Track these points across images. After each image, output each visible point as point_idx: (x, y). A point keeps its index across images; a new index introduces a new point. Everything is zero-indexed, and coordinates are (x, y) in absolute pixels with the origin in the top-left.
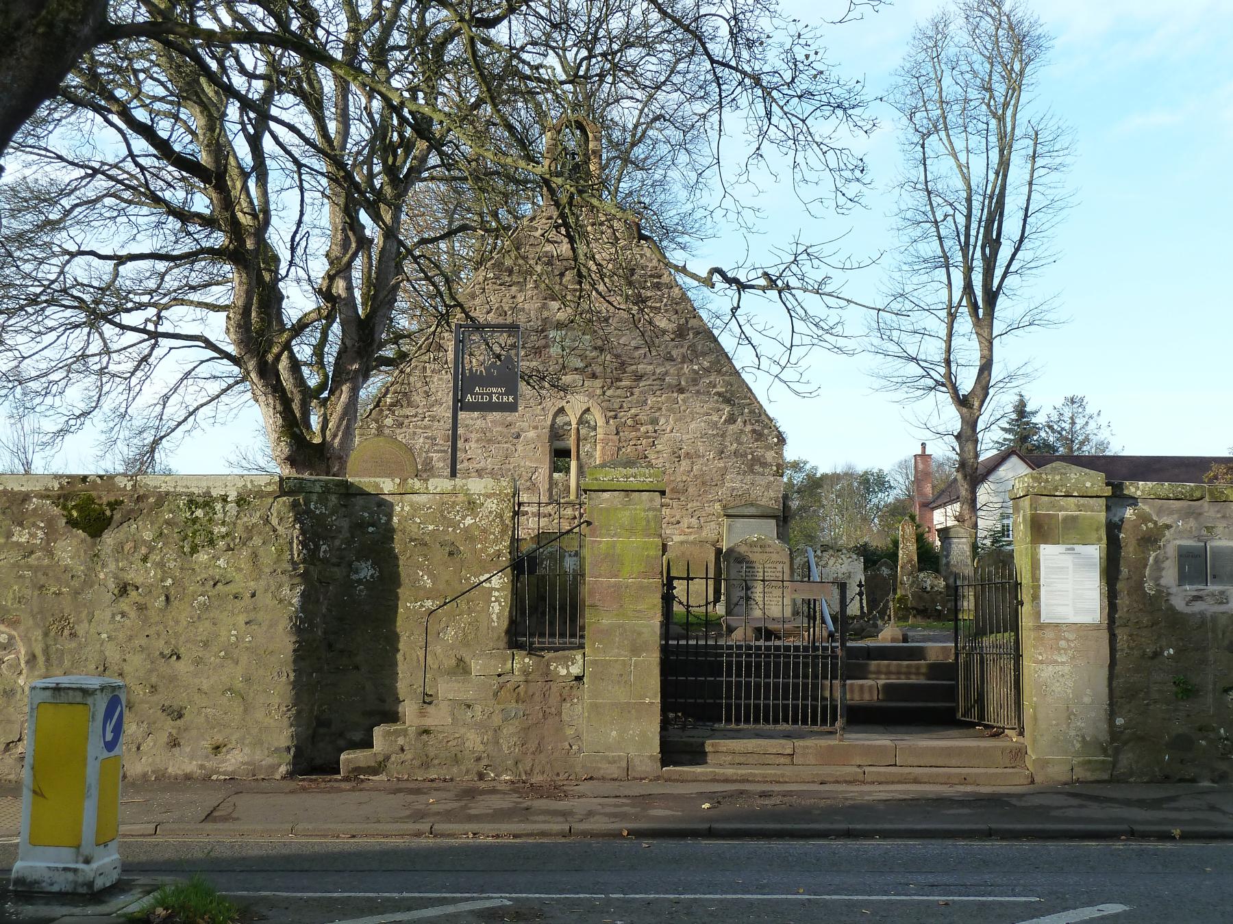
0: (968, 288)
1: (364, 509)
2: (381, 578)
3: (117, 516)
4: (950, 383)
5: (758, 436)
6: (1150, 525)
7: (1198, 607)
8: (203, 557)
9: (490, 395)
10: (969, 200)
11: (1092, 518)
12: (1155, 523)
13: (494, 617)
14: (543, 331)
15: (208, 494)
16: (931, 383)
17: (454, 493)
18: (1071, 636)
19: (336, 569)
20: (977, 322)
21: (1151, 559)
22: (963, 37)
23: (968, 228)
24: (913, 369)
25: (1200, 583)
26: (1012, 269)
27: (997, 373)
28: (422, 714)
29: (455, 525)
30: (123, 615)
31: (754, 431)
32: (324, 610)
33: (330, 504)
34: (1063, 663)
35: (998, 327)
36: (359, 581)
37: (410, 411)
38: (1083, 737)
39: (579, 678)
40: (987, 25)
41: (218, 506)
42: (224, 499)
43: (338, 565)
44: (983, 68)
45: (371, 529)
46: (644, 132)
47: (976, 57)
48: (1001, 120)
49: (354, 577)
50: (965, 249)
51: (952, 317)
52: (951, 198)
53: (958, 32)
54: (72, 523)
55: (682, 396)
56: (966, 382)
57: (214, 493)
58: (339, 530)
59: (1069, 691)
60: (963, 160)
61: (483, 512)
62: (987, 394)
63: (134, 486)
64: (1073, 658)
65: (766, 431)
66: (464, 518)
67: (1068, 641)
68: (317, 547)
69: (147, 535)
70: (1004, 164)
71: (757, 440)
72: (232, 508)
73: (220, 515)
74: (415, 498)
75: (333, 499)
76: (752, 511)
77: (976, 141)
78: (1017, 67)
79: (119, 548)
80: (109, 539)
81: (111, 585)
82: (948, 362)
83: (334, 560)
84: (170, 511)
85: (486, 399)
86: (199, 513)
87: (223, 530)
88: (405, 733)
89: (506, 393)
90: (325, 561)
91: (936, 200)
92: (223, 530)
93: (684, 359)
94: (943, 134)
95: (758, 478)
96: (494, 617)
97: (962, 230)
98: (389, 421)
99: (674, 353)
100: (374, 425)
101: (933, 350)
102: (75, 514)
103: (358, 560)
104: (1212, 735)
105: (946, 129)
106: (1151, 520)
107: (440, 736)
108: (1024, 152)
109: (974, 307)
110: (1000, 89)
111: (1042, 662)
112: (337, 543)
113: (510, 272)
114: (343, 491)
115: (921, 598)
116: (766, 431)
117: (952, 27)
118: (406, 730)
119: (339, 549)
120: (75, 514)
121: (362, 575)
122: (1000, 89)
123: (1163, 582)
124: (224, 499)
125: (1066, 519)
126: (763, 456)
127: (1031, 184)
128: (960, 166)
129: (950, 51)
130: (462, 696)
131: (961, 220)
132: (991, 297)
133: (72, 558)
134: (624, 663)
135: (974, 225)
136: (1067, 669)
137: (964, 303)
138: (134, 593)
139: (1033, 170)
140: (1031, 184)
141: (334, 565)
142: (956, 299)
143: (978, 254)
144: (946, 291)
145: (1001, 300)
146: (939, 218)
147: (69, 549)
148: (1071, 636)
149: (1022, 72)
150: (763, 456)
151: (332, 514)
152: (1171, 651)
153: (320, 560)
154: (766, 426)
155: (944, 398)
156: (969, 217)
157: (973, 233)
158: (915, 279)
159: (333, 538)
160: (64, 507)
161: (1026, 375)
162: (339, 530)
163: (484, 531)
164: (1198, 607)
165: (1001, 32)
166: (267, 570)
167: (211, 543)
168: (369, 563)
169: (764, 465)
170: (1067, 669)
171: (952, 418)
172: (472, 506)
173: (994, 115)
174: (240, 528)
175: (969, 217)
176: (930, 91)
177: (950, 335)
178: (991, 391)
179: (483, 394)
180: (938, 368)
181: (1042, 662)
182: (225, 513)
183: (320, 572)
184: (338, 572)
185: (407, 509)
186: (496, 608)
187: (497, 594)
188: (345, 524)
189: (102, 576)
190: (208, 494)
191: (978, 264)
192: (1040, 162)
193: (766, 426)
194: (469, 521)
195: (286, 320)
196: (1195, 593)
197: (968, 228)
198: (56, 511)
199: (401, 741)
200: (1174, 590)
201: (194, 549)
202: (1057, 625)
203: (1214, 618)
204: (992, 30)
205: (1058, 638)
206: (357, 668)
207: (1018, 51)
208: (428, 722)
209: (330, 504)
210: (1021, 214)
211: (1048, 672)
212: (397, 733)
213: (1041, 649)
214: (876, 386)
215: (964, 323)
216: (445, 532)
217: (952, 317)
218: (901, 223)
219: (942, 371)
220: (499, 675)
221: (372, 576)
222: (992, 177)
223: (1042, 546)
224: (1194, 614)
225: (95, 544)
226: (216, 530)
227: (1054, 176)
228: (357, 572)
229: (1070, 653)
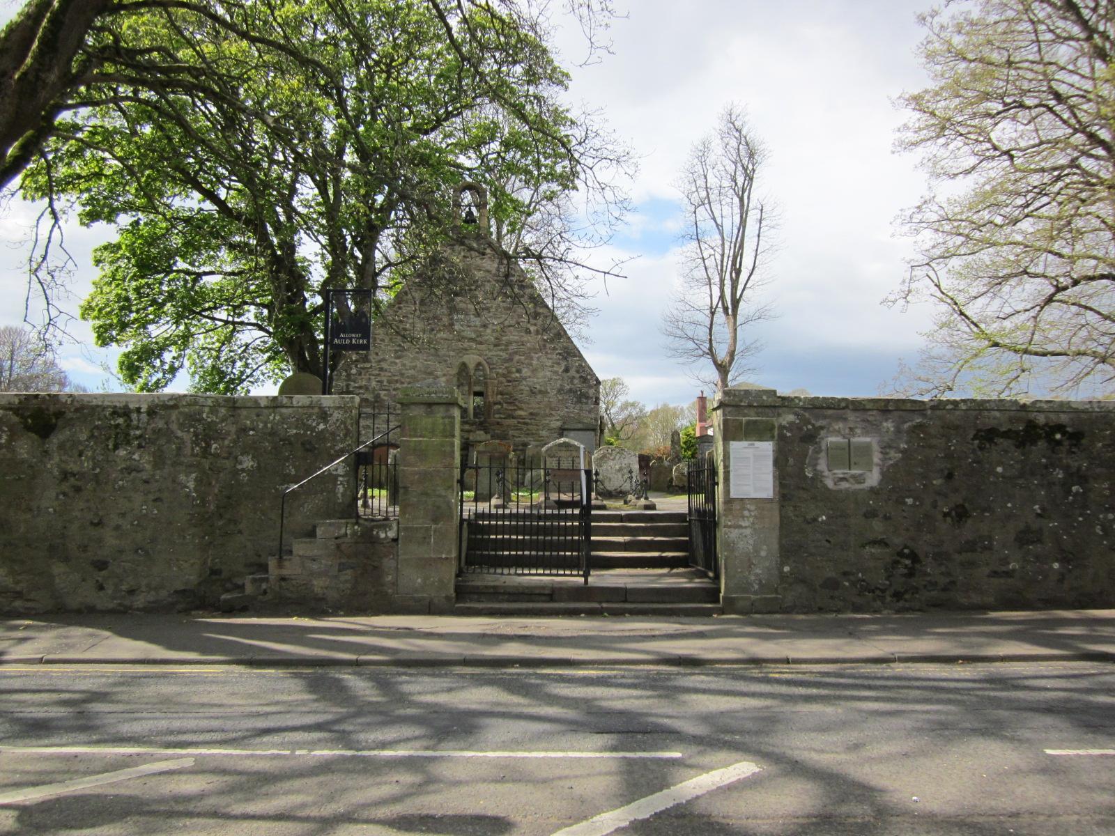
0: (722, 297)
1: (247, 418)
2: (259, 467)
3: (60, 423)
4: (711, 352)
5: (584, 380)
6: (810, 427)
7: (844, 485)
8: (122, 452)
9: (351, 339)
10: (723, 245)
11: (767, 421)
12: (813, 425)
13: (339, 495)
15: (126, 407)
16: (701, 353)
17: (310, 406)
18: (753, 508)
19: (226, 461)
21: (810, 451)
22: (720, 151)
23: (722, 262)
24: (691, 345)
25: (844, 469)
26: (748, 285)
27: (739, 347)
28: (280, 566)
29: (313, 429)
30: (65, 494)
32: (216, 491)
33: (220, 415)
34: (746, 527)
35: (740, 319)
36: (243, 470)
37: (368, 365)
38: (761, 581)
39: (395, 540)
40: (734, 143)
41: (134, 416)
42: (138, 410)
43: (227, 458)
44: (731, 168)
45: (251, 433)
46: (535, 207)
47: (727, 162)
48: (741, 200)
49: (239, 467)
50: (721, 273)
51: (713, 313)
52: (713, 244)
53: (717, 148)
54: (28, 428)
56: (722, 355)
57: (132, 406)
58: (228, 433)
59: (751, 547)
60: (719, 222)
61: (332, 420)
63: (72, 401)
64: (753, 524)
66: (318, 424)
67: (749, 511)
68: (209, 446)
69: (83, 437)
70: (743, 222)
72: (144, 417)
73: (135, 423)
74: (284, 410)
75: (223, 411)
76: (580, 426)
77: (727, 210)
78: (750, 167)
79: (61, 447)
80: (55, 440)
81: (56, 472)
82: (711, 340)
83: (224, 455)
84: (99, 419)
85: (348, 342)
86: (121, 421)
87: (138, 432)
88: (266, 580)
89: (362, 338)
90: (216, 456)
91: (703, 246)
92: (138, 432)
94: (707, 206)
95: (584, 406)
96: (339, 495)
97: (719, 263)
98: (354, 371)
100: (344, 373)
102: (30, 421)
103: (242, 454)
104: (852, 578)
105: (709, 203)
106: (810, 423)
107: (294, 582)
108: (755, 217)
109: (726, 309)
110: (740, 180)
111: (730, 527)
112: (226, 442)
114: (231, 405)
115: (681, 479)
117: (713, 144)
118: (267, 578)
119: (228, 447)
120: (30, 421)
121: (245, 466)
122: (740, 180)
123: (819, 468)
124: (138, 410)
125: (748, 423)
127: (759, 236)
128: (717, 225)
129: (712, 158)
130: (309, 553)
131: (718, 257)
132: (736, 303)
133: (28, 453)
134: (428, 529)
135: (725, 259)
136: (748, 531)
138: (72, 479)
139: (760, 228)
140: (759, 236)
141: (224, 458)
145: (742, 305)
146: (706, 256)
147: (24, 448)
148: (753, 508)
149: (754, 170)
151: (223, 421)
152: (824, 518)
153: (211, 454)
154: (589, 374)
155: (708, 361)
156: (723, 255)
157: (725, 264)
158: (691, 292)
159: (223, 439)
160: (22, 416)
161: (757, 348)
162: (228, 433)
163: (333, 434)
164: (844, 485)
165: (741, 147)
166: (169, 462)
167: (129, 443)
168: (250, 457)
169: (587, 398)
170: (748, 531)
171: (713, 374)
172: (324, 415)
173: (738, 195)
174: (149, 431)
175: (723, 255)
176: (701, 182)
178: (736, 358)
179: (345, 339)
181: (730, 527)
182: (139, 420)
183: (211, 464)
184: (228, 464)
185: (277, 418)
186: (341, 489)
187: (341, 479)
188: (233, 429)
189: (49, 466)
190: (126, 407)
191: (728, 283)
192: (764, 223)
194: (322, 426)
196: (841, 476)
197: (722, 262)
198: (15, 419)
199: (264, 586)
200: (826, 473)
201: (116, 447)
202: (742, 499)
203: (855, 493)
204: (735, 145)
205: (744, 509)
206: (240, 532)
207: (751, 155)
208: (285, 572)
209: (220, 415)
210: (754, 254)
211: (734, 534)
212: (262, 580)
213: (730, 517)
214: (669, 355)
215: (720, 317)
216: (305, 434)
217: (713, 313)
218: (684, 259)
219: (708, 346)
220: (336, 538)
221: (252, 466)
222: (735, 231)
223: (731, 442)
224: (840, 491)
225: (44, 444)
226: (132, 433)
227: (773, 231)
228: (241, 463)
229: (751, 519)
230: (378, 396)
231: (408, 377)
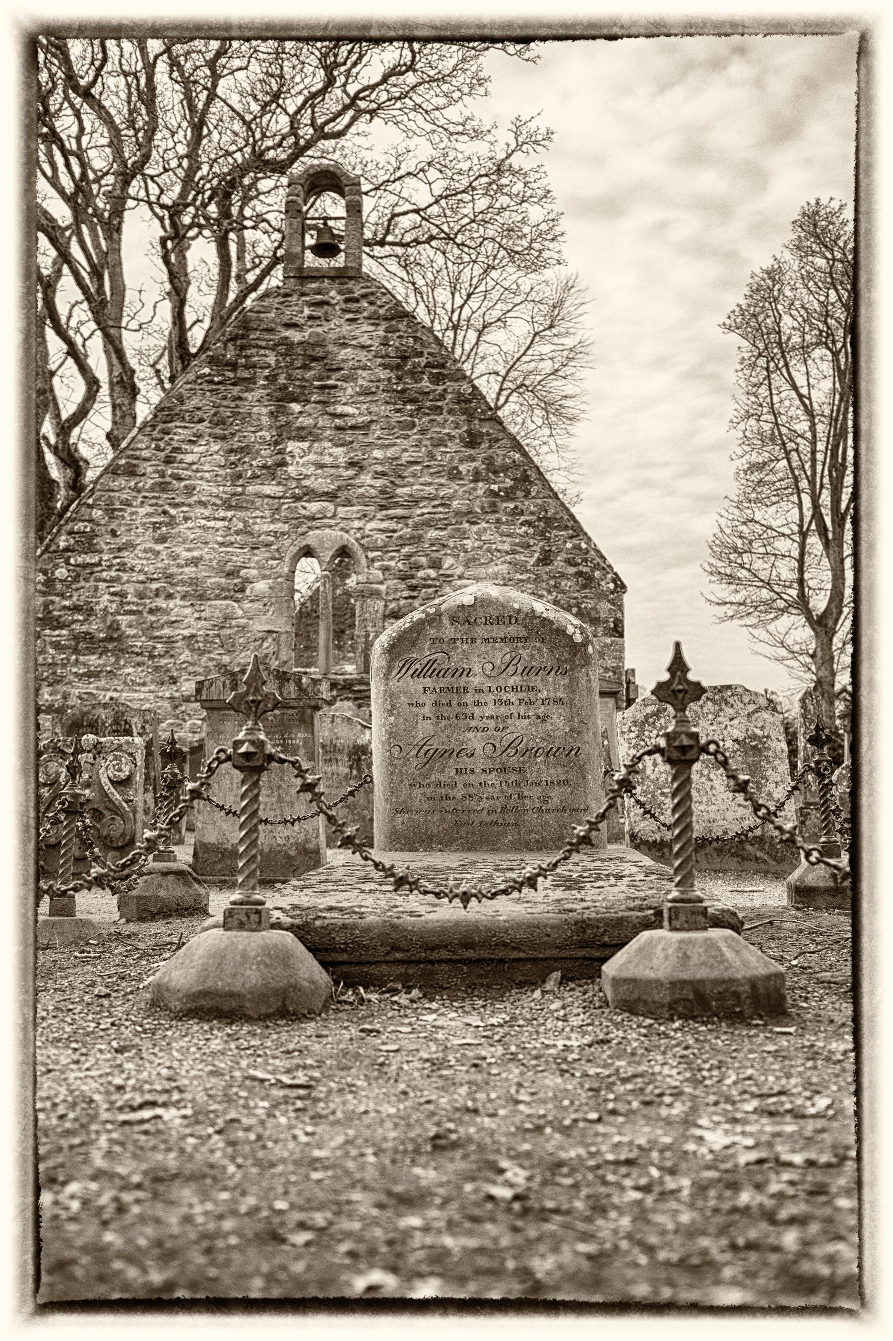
0: (817, 515)
4: (802, 603)
5: (587, 581)
14: (276, 443)
20: (827, 544)
31: (580, 574)
51: (804, 535)
55: (475, 528)
56: (819, 603)
62: (841, 612)
65: (597, 574)
71: (584, 587)
93: (477, 477)
99: (463, 468)
101: (786, 570)
113: (234, 366)
116: (597, 574)
126: (594, 609)
128: (801, 396)
137: (813, 527)
142: (807, 520)
143: (826, 480)
144: (796, 511)
150: (594, 609)
154: (597, 567)
177: (802, 554)
180: (789, 591)
193: (597, 567)
195: (822, 884)
215: (814, 542)
217: (804, 535)
230: (114, 627)
231: (183, 583)
